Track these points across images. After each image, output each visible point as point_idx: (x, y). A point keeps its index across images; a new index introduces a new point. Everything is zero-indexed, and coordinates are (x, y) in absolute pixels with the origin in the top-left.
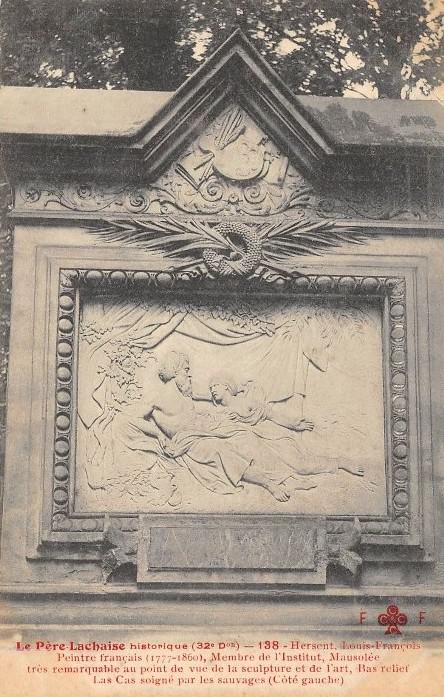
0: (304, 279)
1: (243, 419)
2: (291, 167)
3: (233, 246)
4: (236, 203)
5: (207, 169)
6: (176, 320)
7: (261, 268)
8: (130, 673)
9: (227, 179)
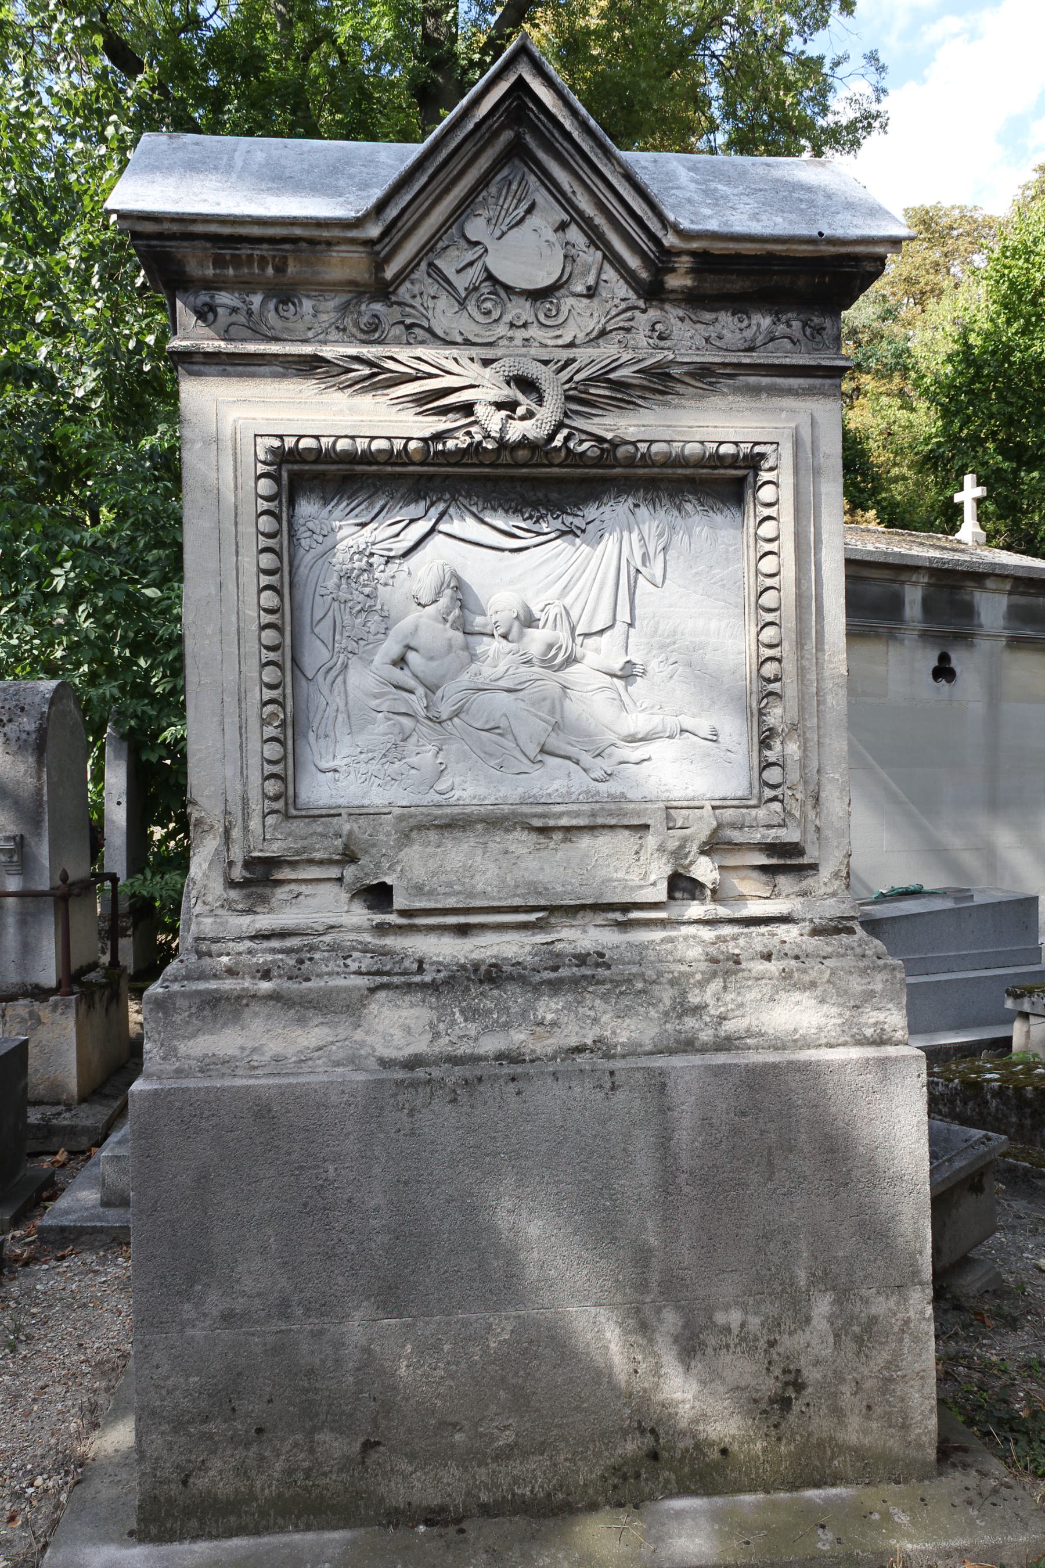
2: (607, 266)
3: (520, 397)
4: (525, 325)
5: (474, 274)
6: (434, 513)
7: (565, 432)
9: (508, 289)
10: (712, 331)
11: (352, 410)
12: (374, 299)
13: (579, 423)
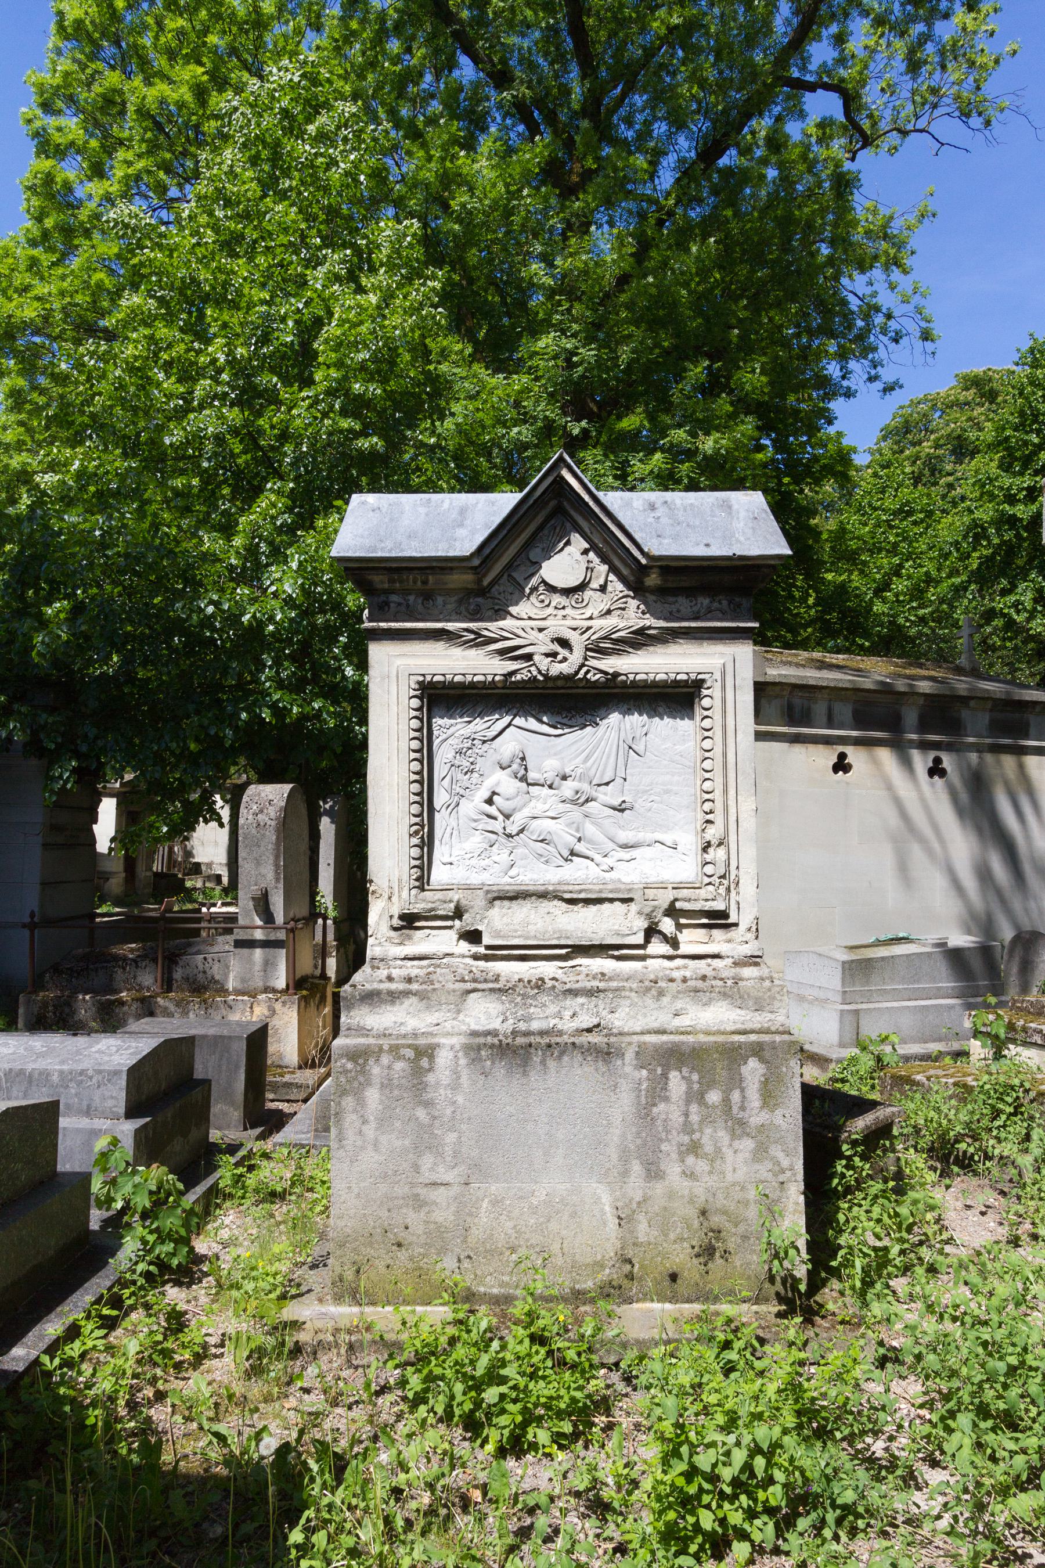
1: (574, 802)
3: (559, 649)
8: (232, 1249)
10: (674, 608)
11: (464, 658)
12: (477, 595)
13: (593, 663)
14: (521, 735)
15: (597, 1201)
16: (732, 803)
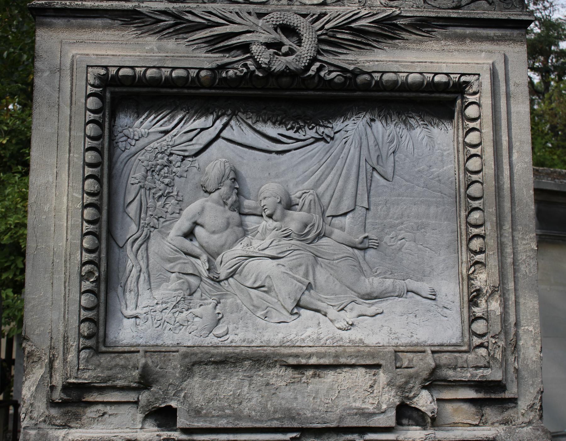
0: (367, 77)
3: (285, 40)
6: (219, 124)
7: (318, 64)
14: (232, 145)
15: (108, 22)
16: (507, 241)
